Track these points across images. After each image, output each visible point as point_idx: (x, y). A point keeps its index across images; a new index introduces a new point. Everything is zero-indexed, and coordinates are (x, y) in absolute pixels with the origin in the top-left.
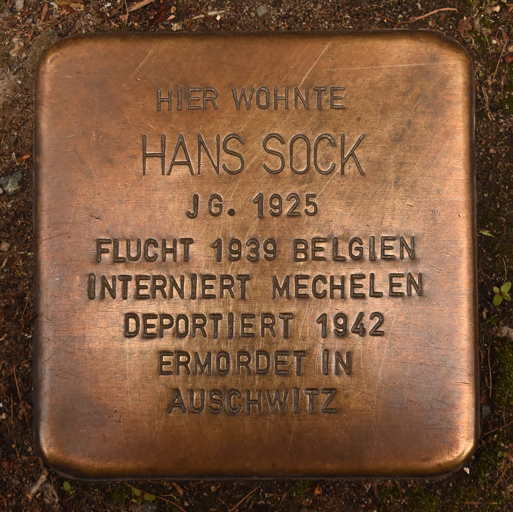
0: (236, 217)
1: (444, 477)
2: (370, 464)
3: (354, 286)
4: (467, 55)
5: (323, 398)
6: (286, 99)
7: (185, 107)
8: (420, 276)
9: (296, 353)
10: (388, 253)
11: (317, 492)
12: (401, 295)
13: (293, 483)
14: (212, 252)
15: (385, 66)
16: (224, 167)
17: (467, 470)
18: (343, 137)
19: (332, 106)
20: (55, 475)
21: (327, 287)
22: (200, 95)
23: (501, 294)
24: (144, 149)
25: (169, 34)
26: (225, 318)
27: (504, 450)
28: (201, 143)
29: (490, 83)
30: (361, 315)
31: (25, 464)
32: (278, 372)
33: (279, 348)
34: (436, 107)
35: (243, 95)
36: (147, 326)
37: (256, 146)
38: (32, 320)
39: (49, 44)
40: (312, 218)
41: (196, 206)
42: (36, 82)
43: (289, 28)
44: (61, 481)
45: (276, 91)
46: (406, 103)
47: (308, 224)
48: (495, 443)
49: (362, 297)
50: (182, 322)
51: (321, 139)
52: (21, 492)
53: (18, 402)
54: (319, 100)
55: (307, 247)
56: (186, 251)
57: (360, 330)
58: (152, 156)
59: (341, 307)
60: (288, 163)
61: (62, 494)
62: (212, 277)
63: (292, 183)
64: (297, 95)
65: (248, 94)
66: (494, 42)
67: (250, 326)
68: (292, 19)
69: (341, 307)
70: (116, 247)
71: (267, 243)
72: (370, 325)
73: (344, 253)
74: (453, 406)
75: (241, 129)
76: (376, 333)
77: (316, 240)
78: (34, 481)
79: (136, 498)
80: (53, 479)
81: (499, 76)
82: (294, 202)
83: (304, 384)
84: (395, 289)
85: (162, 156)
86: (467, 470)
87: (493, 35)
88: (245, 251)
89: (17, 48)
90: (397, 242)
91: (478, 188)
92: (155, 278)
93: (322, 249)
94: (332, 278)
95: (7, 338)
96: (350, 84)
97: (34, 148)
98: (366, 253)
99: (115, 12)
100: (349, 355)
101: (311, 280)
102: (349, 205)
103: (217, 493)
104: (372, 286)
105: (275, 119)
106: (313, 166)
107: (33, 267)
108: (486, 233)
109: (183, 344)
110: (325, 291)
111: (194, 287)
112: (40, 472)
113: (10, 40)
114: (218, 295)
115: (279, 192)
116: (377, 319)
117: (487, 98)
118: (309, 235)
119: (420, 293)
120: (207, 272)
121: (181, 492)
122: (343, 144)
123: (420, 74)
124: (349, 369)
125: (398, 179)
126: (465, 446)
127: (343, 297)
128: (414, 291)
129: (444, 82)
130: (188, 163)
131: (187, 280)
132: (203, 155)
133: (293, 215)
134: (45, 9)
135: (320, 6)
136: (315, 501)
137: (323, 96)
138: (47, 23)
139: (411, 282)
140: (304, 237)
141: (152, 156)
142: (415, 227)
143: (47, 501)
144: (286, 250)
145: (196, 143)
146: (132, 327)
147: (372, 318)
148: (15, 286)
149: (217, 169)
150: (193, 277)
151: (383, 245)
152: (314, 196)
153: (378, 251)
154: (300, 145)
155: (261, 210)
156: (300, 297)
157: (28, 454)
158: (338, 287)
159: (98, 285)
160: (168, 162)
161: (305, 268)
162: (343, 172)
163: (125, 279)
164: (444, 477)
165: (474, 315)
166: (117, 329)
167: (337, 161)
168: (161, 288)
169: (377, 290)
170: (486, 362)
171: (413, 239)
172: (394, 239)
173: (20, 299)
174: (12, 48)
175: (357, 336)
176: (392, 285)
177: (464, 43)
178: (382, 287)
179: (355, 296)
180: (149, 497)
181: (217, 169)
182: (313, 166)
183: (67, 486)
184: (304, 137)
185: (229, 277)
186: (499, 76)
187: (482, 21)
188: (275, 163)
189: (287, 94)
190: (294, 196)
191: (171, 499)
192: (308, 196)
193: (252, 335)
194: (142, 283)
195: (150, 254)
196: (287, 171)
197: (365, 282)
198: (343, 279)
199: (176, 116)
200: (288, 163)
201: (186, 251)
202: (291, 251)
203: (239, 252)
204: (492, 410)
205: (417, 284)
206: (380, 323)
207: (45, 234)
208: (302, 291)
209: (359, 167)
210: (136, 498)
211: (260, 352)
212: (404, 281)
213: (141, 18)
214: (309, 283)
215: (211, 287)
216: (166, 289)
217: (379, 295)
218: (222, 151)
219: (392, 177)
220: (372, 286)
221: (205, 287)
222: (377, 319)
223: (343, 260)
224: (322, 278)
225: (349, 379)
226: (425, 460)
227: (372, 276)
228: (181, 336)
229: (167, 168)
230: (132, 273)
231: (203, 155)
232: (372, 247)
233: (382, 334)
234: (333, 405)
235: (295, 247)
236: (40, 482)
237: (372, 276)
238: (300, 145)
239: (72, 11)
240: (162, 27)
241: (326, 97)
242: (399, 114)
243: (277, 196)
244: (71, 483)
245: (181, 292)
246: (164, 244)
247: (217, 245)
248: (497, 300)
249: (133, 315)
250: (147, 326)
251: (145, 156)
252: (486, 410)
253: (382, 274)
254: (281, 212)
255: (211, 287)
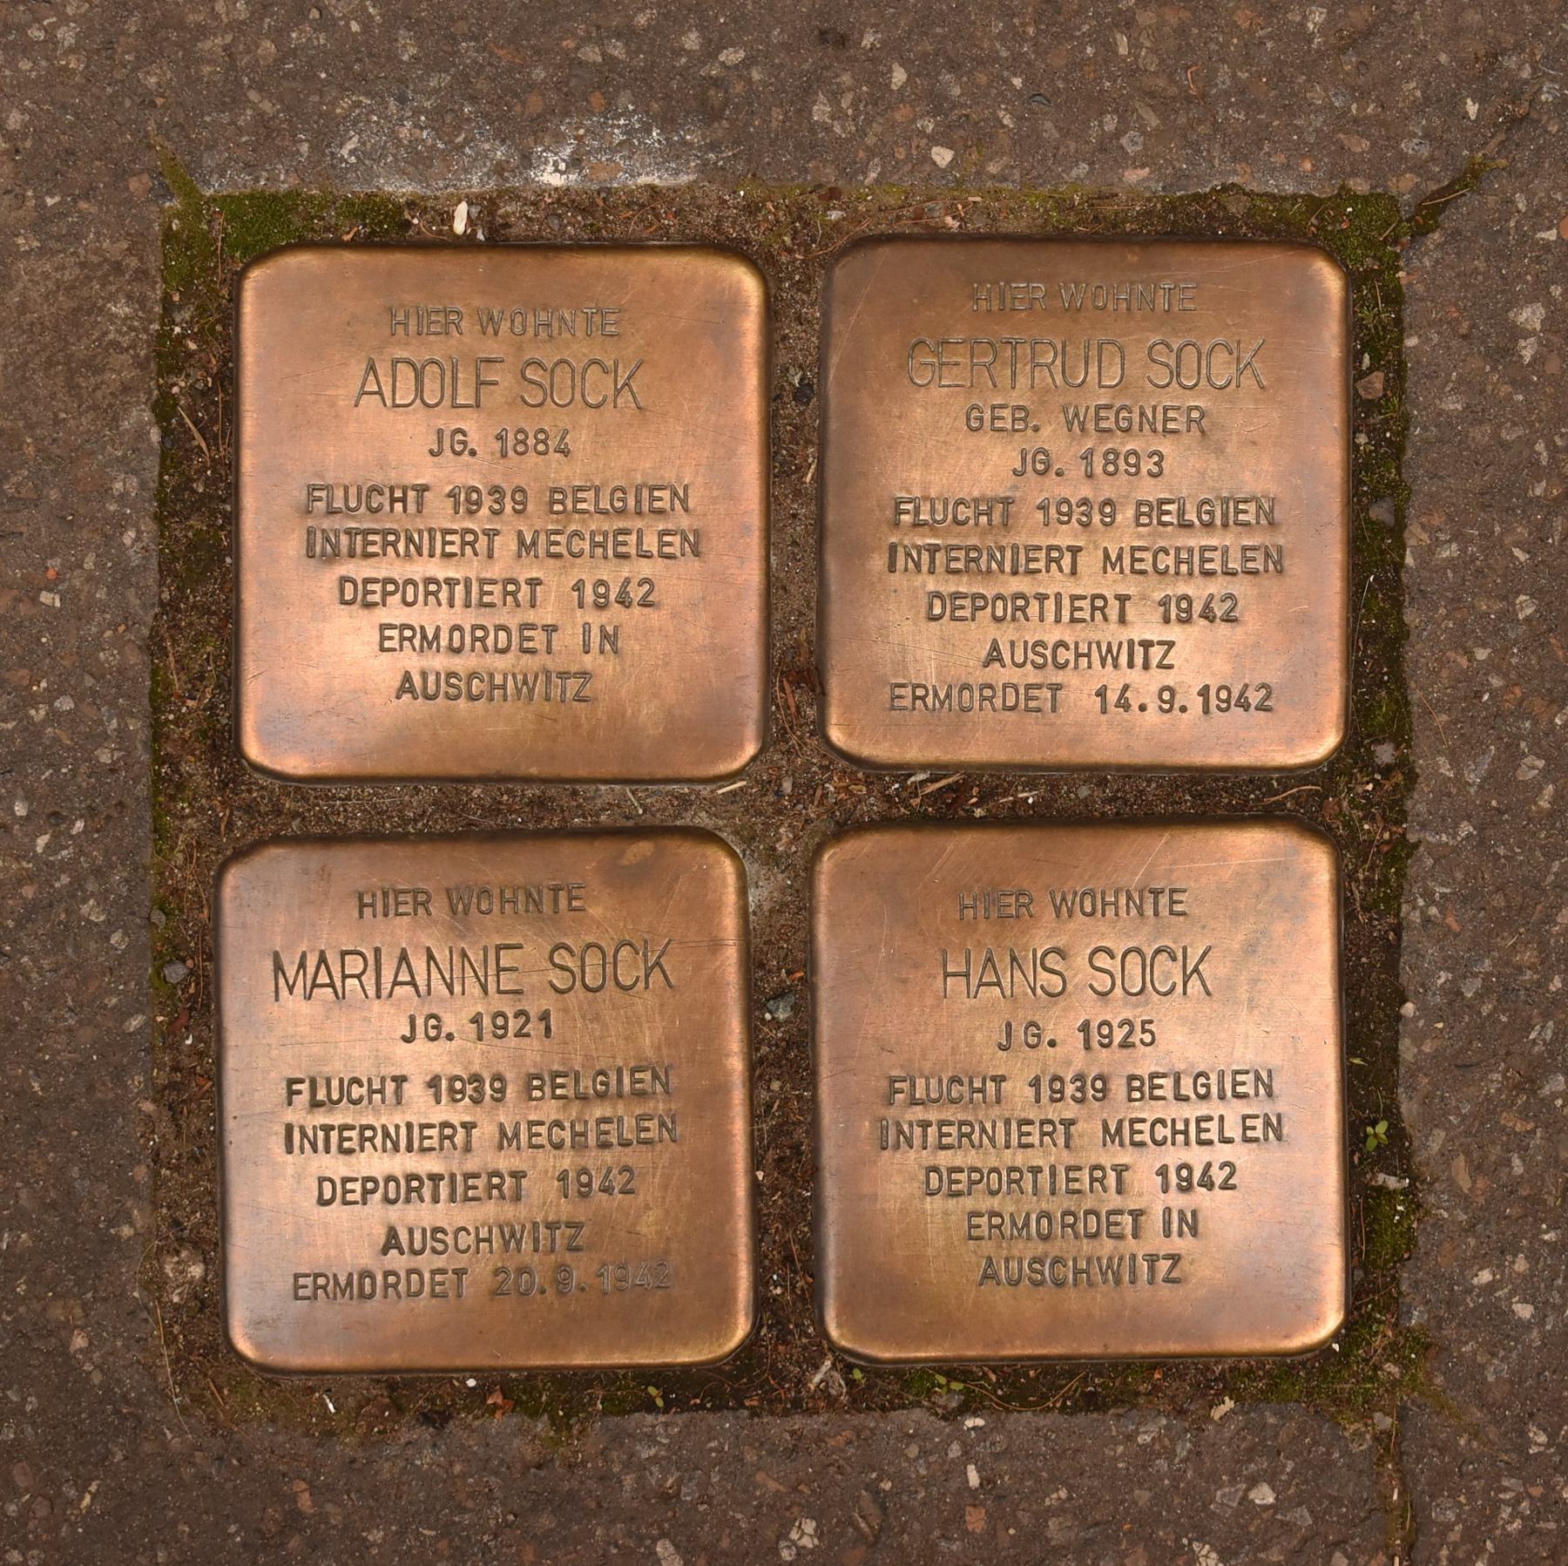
0: (1058, 1048)
1: (1309, 1355)
2: (1221, 1345)
3: (1199, 1130)
4: (1334, 847)
5: (1164, 1266)
6: (1116, 904)
7: (994, 915)
8: (1279, 1117)
9: (1131, 1213)
10: (1240, 1089)
11: (1157, 1376)
12: (1256, 1140)
13: (1129, 1365)
14: (1030, 1092)
15: (1235, 862)
16: (1042, 987)
17: (1336, 1347)
18: (1185, 949)
19: (1172, 913)
20: (843, 1360)
21: (1168, 1132)
22: (1012, 899)
23: (1376, 1135)
24: (945, 966)
25: (970, 823)
26: (1047, 1171)
27: (1380, 1322)
28: (1014, 959)
29: (1361, 877)
30: (1209, 1165)
31: (805, 1348)
32: (1109, 1236)
33: (1111, 1207)
34: (1296, 909)
35: (1064, 899)
36: (952, 1182)
37: (1082, 960)
38: (813, 1174)
39: (824, 834)
40: (1148, 1049)
41: (1009, 1035)
42: (810, 883)
43: (1117, 813)
44: (849, 1368)
45: (1103, 893)
46: (1260, 906)
47: (1144, 1056)
48: (1370, 1315)
49: (1210, 1143)
50: (994, 1176)
51: (1158, 951)
52: (801, 1382)
53: (796, 1272)
54: (1156, 904)
55: (1143, 1084)
56: (998, 1090)
57: (1207, 1183)
58: (954, 975)
59: (1183, 588)
60: (1119, 982)
61: (851, 1383)
62: (1030, 1123)
63: (1126, 1004)
64: (1129, 898)
65: (1070, 898)
66: (1366, 827)
67: (1076, 1180)
68: (1120, 802)
69: (1183, 588)
70: (913, 1086)
71: (1095, 1079)
72: (1219, 1176)
73: (1191, 516)
74: (1319, 1272)
75: (1060, 942)
76: (1226, 1186)
77: (1153, 1076)
78: (817, 1368)
79: (940, 1386)
80: (840, 1366)
81: (1372, 869)
82: (1126, 1028)
83: (1141, 1249)
84: (1250, 1134)
85: (967, 975)
86: (1336, 1347)
87: (1365, 818)
88: (1070, 1089)
89: (785, 840)
90: (1251, 1076)
91: (1348, 1006)
92: (961, 1124)
93: (1161, 1087)
94: (1174, 1121)
95: (782, 1197)
96: (1192, 884)
97: (809, 963)
98: (1214, 1090)
99: (904, 795)
100: (1194, 1213)
101: (1148, 1124)
102: (1193, 1031)
103: (1037, 1377)
104: (1221, 1130)
105: (1103, 929)
106: (1149, 985)
107: (812, 1107)
108: (1357, 1061)
109: (995, 1203)
110: (1165, 1138)
111: (1008, 1134)
112: (823, 1355)
113: (777, 832)
114: (1037, 1143)
115: (1108, 1018)
116: (1227, 1170)
117: (1357, 895)
118: (1144, 1070)
119: (1279, 1138)
120: (1023, 1115)
121: (993, 1377)
122: (1185, 957)
123: (1272, 873)
124: (1194, 1231)
125: (1251, 1000)
126: (1332, 1319)
127: (1190, 574)
128: (1271, 1135)
129: (1305, 880)
130: (998, 984)
131: (1000, 1126)
132: (1017, 974)
133: (1125, 1045)
134: (819, 793)
135: (1154, 785)
136: (1154, 1386)
137: (1159, 900)
138: (821, 810)
139: (1267, 1123)
140: (1138, 1072)
141: (954, 975)
142: (1274, 1059)
143: (833, 1392)
144: (1118, 1088)
145: (1008, 959)
146: (934, 1183)
147: (1221, 1168)
148: (790, 1134)
149: (1034, 991)
150: (1007, 1122)
151: (1234, 1079)
152: (1151, 1022)
153: (1228, 1087)
154: (1133, 959)
155: (1087, 1041)
156: (1134, 1144)
157: (808, 1336)
158: (1181, 1132)
159: (892, 1131)
160: (974, 981)
161: (1142, 1109)
162: (1185, 993)
163: (925, 1125)
164: (1309, 1355)
165: (1344, 1161)
166: (916, 1185)
167: (1178, 979)
168: (968, 1136)
169: (1228, 1134)
170: (1358, 1217)
171: (1270, 1072)
172: (1247, 1072)
173: (796, 1149)
174: (779, 840)
175: (1204, 1190)
176: (1245, 1128)
177: (1329, 828)
178: (1234, 1130)
179: (1201, 1143)
180: (956, 1386)
181: (1034, 991)
182: (1149, 985)
183: (857, 1374)
184: (1138, 951)
185: (1051, 1122)
186: (1372, 869)
187: (1352, 801)
188: (1103, 983)
189: (1116, 898)
190: (1128, 1022)
191: (982, 1387)
192: (1144, 1023)
193: (1079, 1192)
194: (944, 1129)
195: (954, 1094)
196: (1118, 991)
197: (1213, 1125)
198: (1187, 1122)
199: (983, 926)
200: (1119, 982)
201: (998, 1090)
202: (1124, 1089)
203: (1061, 1092)
204: (1366, 1273)
205: (1275, 1127)
206: (1232, 1174)
207: (825, 1071)
208: (1137, 1138)
209: (1204, 985)
210: (940, 1386)
211: (1087, 1213)
212: (1259, 1123)
213: (935, 801)
214: (1146, 1127)
215: (1029, 1134)
216: (976, 1137)
217: (1230, 1141)
218: (1039, 969)
219: (1245, 996)
220: (1221, 1130)
221: (1021, 1134)
222: (1227, 1170)
223: (1186, 1099)
224: (1162, 1122)
225: (399, 665)
226: (1286, 1337)
227: (1222, 1118)
228: (993, 1193)
229: (973, 989)
230: (933, 1116)
231: (1017, 974)
232: (1221, 1082)
233: (1233, 1187)
234: (1174, 1275)
235: (1129, 1084)
236: (824, 1369)
237: (1222, 1118)
238: (1133, 959)
239: (851, 794)
240: (962, 813)
241: (1164, 900)
242: (1252, 920)
243: (1106, 1023)
244: (862, 1369)
245: (992, 1140)
246: (971, 1082)
247: (1036, 1083)
248: (1371, 1144)
249: (935, 1169)
250: (952, 1182)
251: (947, 975)
252: (1359, 1274)
253: (1233, 1113)
254: (1111, 1042)
255: (1029, 1134)
